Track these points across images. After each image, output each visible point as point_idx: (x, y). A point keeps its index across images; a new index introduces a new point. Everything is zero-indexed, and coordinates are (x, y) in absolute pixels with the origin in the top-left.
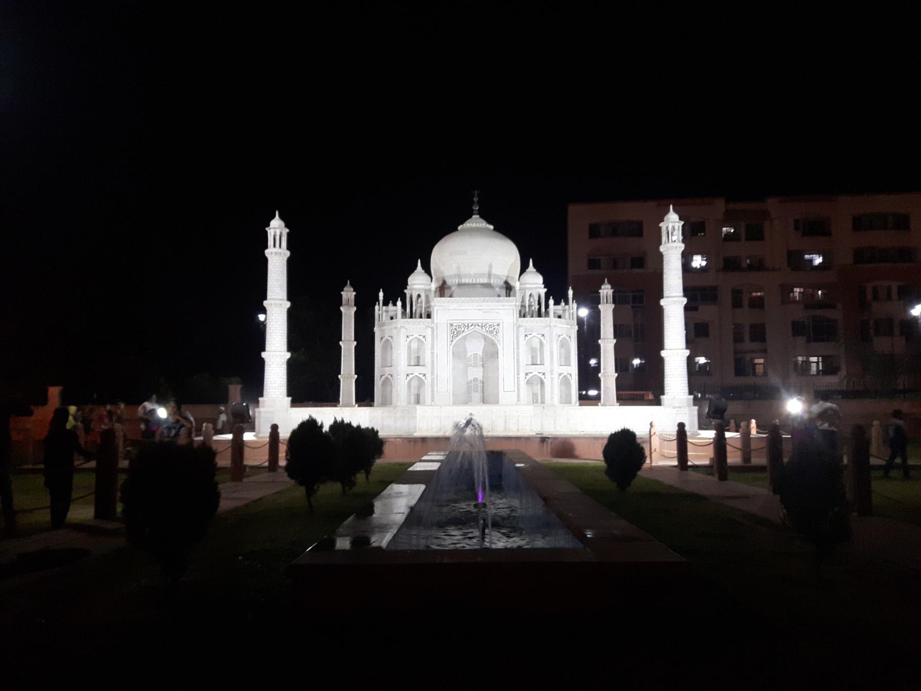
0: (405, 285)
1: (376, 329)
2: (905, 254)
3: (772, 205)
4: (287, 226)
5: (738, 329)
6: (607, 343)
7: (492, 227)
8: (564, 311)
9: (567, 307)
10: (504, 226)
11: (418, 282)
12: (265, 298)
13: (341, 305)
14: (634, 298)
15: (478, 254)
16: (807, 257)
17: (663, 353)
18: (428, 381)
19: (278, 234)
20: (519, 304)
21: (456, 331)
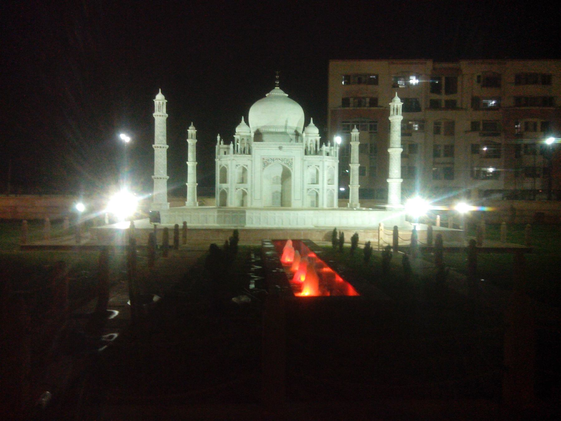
0: (234, 132)
1: (217, 160)
2: (548, 101)
3: (464, 65)
4: (166, 99)
5: (436, 147)
6: (355, 167)
7: (287, 95)
8: (331, 150)
9: (332, 148)
10: (295, 94)
11: (241, 131)
12: (154, 144)
13: (187, 138)
14: (371, 126)
15: (276, 113)
16: (484, 101)
17: (388, 181)
18: (249, 193)
19: (161, 103)
20: (304, 146)
21: (266, 163)
